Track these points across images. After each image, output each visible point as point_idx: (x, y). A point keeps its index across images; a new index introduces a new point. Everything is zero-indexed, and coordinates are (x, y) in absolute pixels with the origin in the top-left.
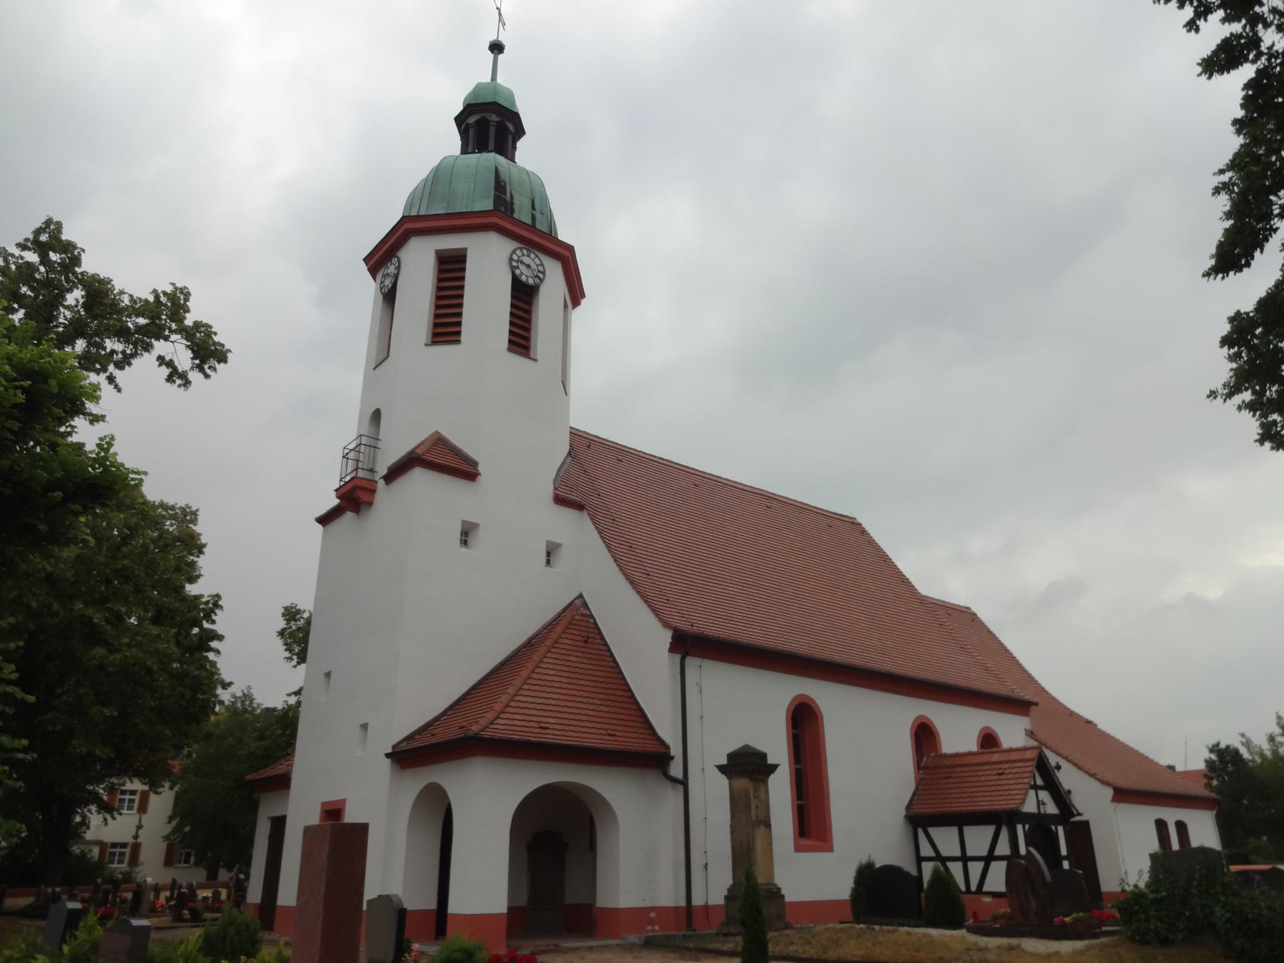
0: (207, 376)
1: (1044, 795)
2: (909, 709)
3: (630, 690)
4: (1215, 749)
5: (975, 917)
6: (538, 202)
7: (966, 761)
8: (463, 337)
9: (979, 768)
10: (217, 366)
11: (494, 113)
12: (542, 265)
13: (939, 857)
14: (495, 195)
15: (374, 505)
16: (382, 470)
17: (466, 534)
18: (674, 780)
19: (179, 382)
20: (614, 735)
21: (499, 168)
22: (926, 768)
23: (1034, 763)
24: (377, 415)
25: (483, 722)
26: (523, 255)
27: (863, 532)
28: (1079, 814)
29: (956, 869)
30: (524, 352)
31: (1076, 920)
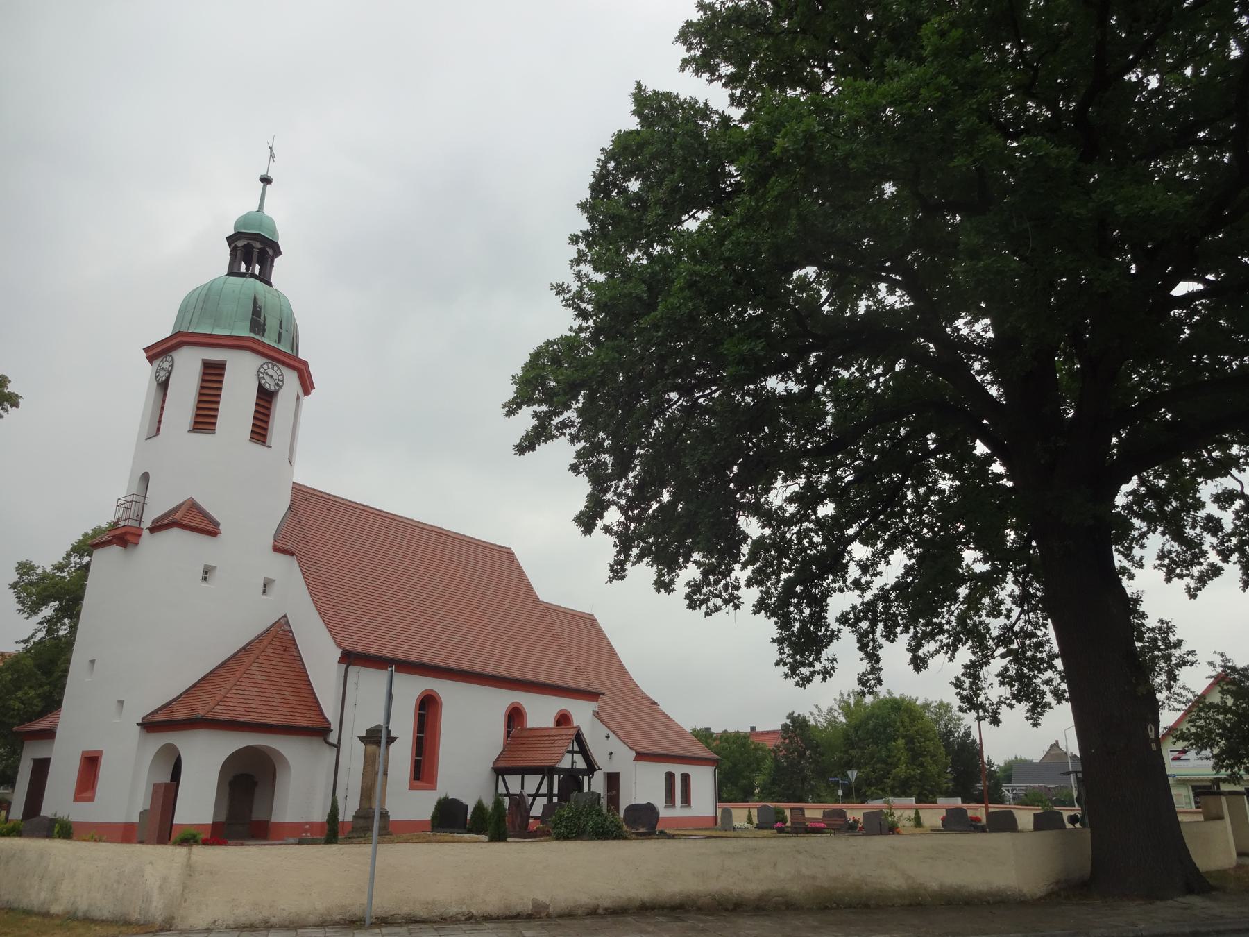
2: (504, 699)
6: (287, 328)
7: (546, 733)
9: (539, 739)
12: (282, 375)
14: (252, 318)
16: (147, 523)
17: (206, 575)
20: (295, 716)
23: (574, 738)
24: (145, 477)
25: (207, 708)
26: (269, 368)
30: (262, 439)
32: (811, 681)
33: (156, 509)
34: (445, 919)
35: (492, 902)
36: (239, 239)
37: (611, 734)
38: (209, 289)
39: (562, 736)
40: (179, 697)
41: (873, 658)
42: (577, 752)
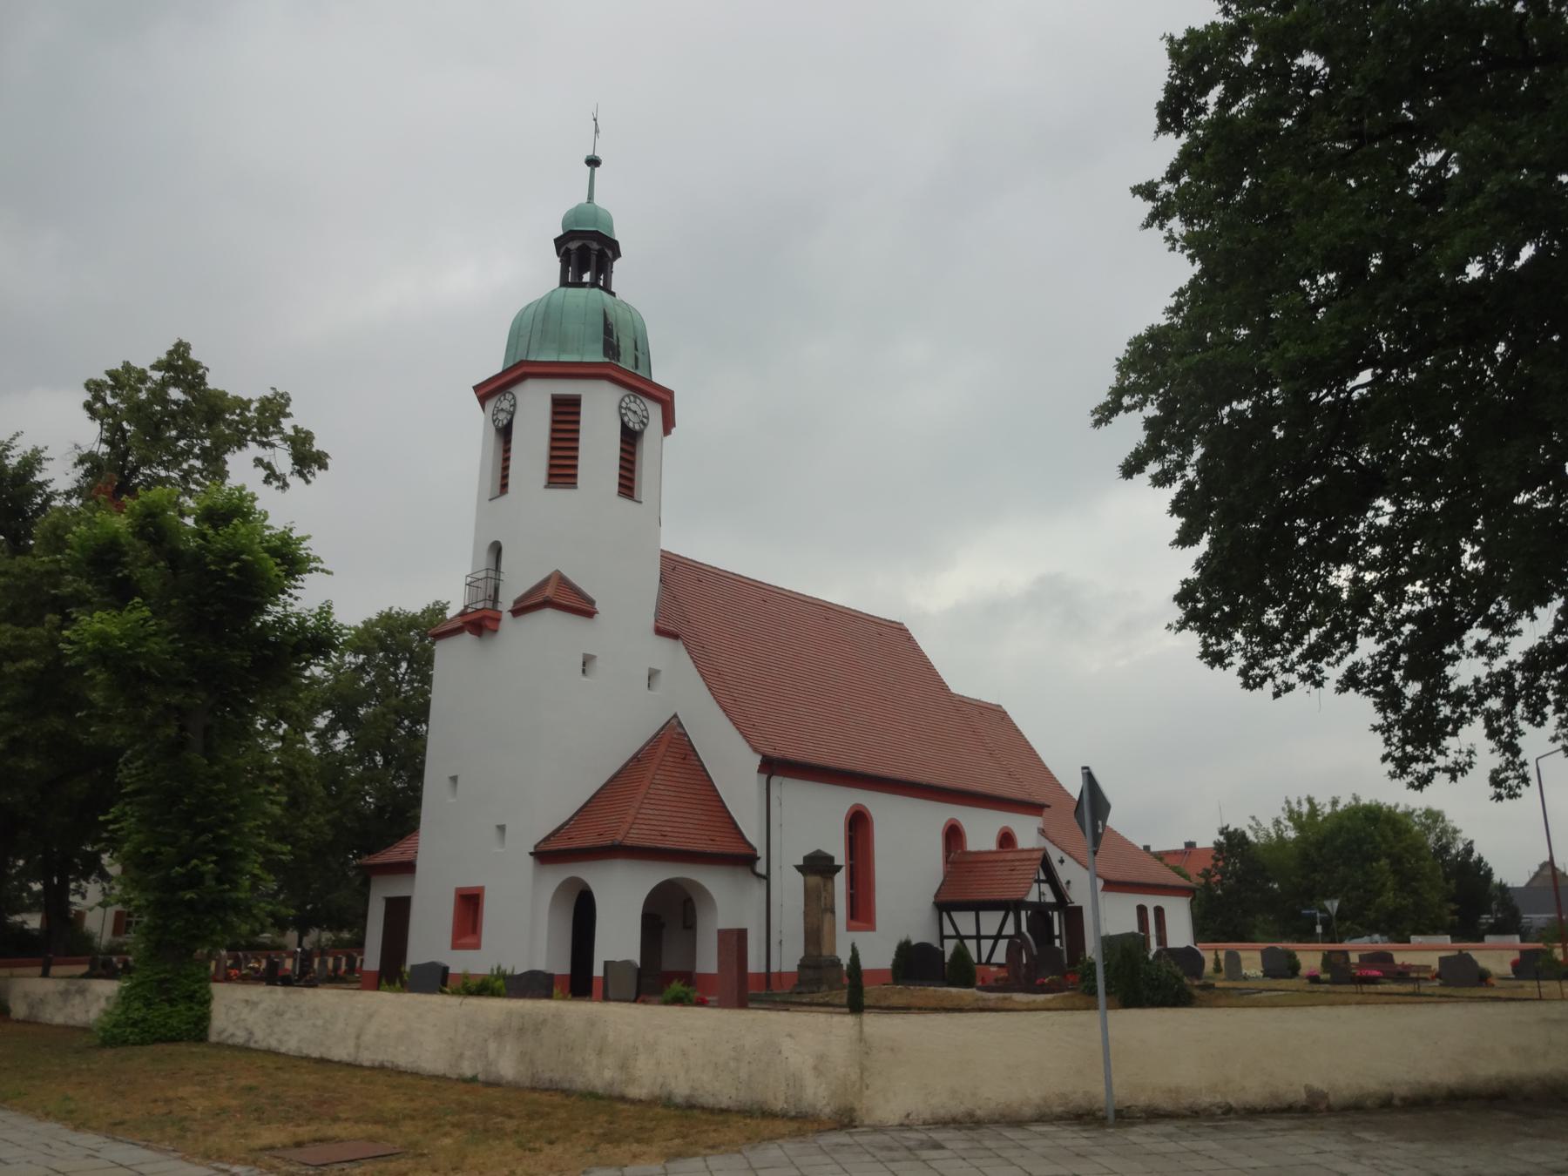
0: (308, 482)
1: (1046, 888)
3: (722, 801)
4: (1223, 831)
5: (983, 980)
8: (579, 484)
10: (317, 471)
11: (594, 240)
12: (646, 410)
13: (961, 938)
15: (500, 631)
16: (506, 603)
17: (587, 661)
18: (759, 876)
19: (275, 484)
21: (607, 310)
22: (953, 863)
23: (1040, 862)
24: (496, 549)
27: (910, 638)
28: (1072, 903)
29: (971, 945)
31: (1051, 981)
32: (1430, 781)
33: (517, 582)
34: (1196, 1112)
35: (1252, 1090)
36: (572, 239)
37: (1066, 858)
38: (548, 305)
39: (1024, 860)
40: (571, 819)
41: (1511, 748)
42: (1043, 881)
